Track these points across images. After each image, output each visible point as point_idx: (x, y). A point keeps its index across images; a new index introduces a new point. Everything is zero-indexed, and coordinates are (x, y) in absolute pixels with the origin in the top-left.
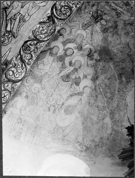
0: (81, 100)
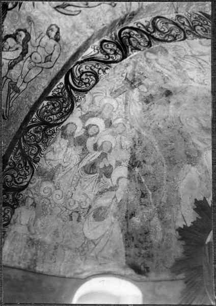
0: (115, 197)
